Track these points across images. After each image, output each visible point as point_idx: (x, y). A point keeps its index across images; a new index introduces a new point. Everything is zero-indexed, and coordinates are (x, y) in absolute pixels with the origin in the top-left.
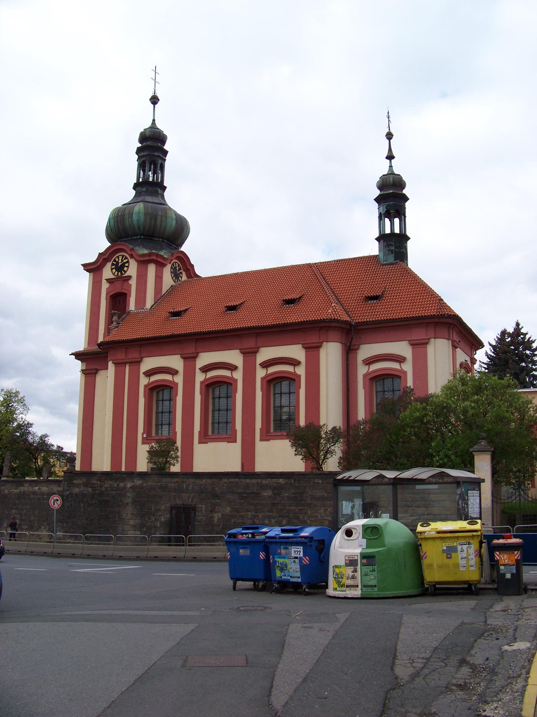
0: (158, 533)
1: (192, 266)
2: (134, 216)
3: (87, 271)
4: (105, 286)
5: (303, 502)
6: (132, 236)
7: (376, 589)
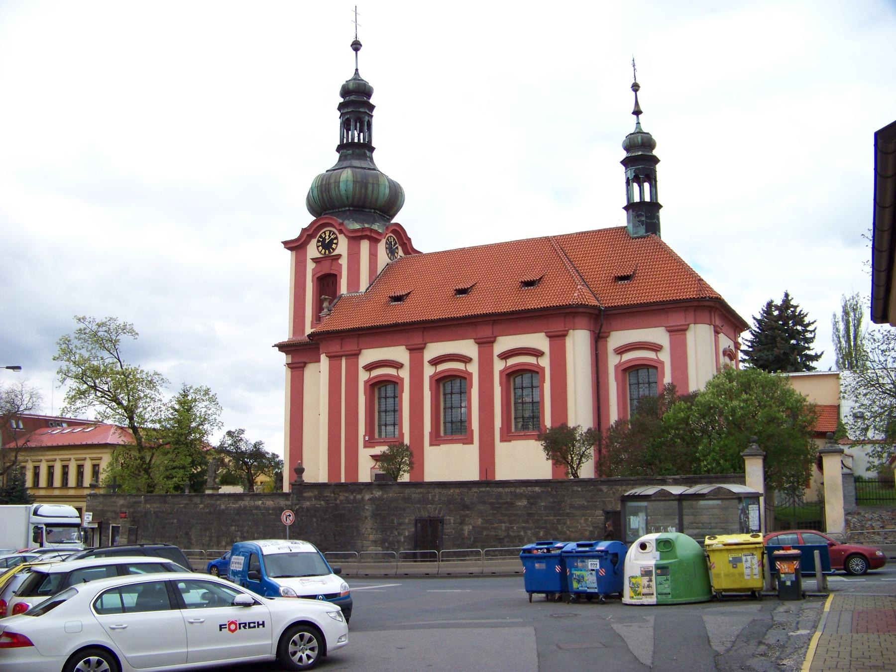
0: (402, 548)
1: (409, 240)
2: (341, 185)
3: (289, 249)
4: (310, 266)
5: (561, 512)
6: (339, 208)
7: (670, 596)
